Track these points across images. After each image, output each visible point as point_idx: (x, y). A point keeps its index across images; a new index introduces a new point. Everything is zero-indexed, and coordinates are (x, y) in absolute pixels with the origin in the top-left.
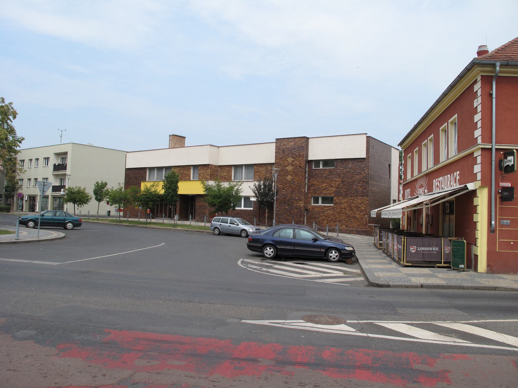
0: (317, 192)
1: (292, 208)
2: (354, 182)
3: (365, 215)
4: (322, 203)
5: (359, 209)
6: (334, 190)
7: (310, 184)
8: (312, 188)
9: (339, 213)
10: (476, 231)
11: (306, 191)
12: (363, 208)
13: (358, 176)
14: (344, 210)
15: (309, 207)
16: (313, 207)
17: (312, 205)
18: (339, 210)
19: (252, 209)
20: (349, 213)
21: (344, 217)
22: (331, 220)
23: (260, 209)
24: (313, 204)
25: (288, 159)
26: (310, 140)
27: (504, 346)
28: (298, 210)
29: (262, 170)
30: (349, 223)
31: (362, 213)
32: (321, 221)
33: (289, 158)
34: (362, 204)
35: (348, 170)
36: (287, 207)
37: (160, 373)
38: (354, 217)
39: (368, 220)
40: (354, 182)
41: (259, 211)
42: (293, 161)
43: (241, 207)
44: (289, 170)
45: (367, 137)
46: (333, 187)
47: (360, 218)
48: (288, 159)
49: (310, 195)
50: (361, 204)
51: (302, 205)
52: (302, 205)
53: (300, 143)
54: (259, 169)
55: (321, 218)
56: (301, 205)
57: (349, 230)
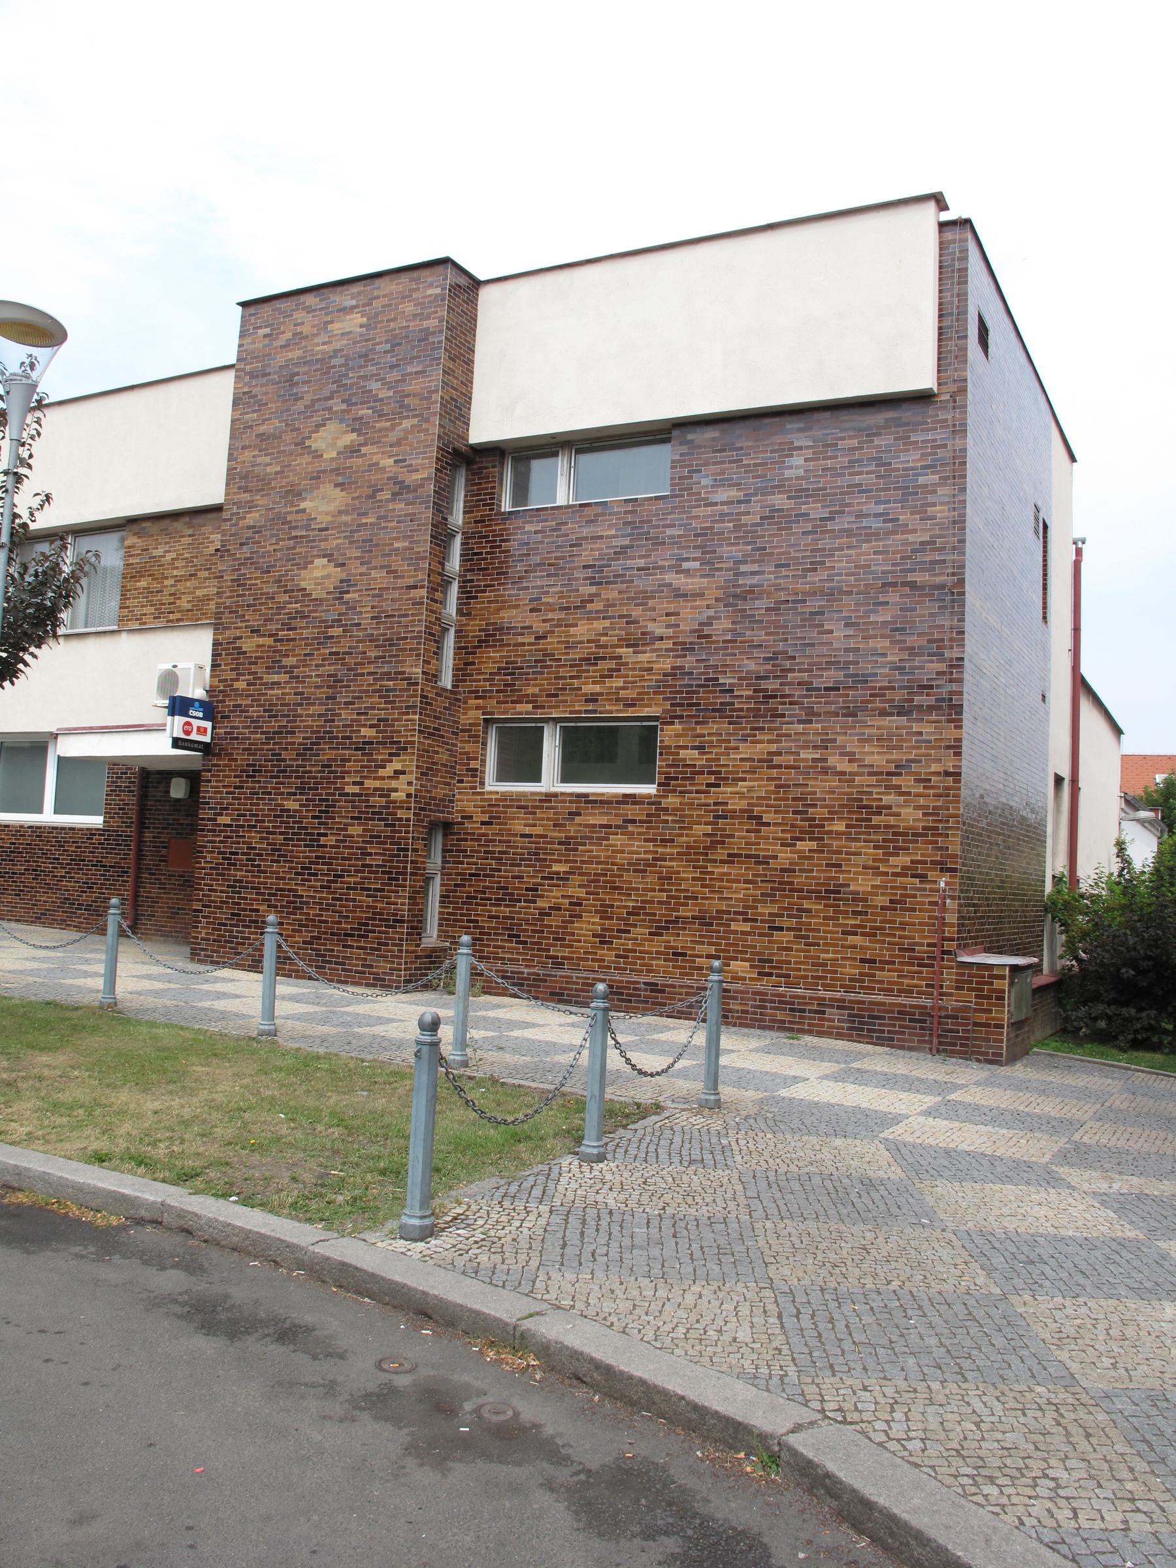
0: (531, 690)
1: (326, 812)
3: (931, 875)
4: (567, 776)
5: (876, 820)
6: (666, 664)
7: (475, 627)
8: (491, 659)
9: (697, 854)
11: (447, 681)
12: (911, 817)
14: (740, 837)
15: (465, 802)
16: (498, 809)
17: (488, 788)
18: (700, 830)
19: (97, 821)
20: (785, 856)
21: (739, 892)
22: (634, 912)
23: (142, 825)
24: (493, 785)
25: (319, 441)
26: (485, 294)
28: (378, 826)
29: (169, 556)
30: (785, 937)
32: (554, 921)
33: (323, 432)
34: (906, 782)
35: (779, 500)
36: (292, 805)
37: (191, 1233)
38: (832, 893)
39: (952, 918)
40: (832, 595)
41: (140, 833)
42: (353, 451)
43: (41, 812)
44: (324, 520)
45: (943, 225)
46: (658, 645)
47: (881, 900)
48: (319, 441)
49: (471, 715)
50: (895, 781)
51: (401, 783)
52: (401, 790)
53: (409, 308)
54: (155, 553)
55: (553, 896)
56: (394, 784)
57: (782, 1002)
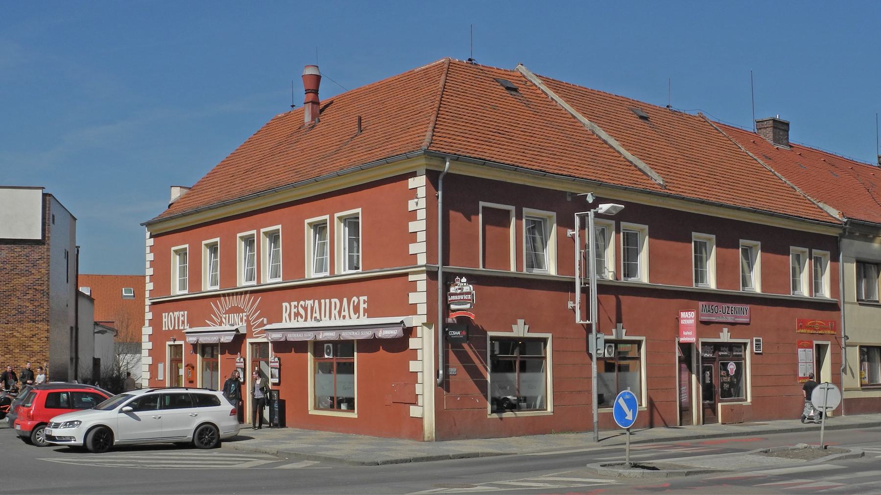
2: (14, 290)
5: (27, 349)
10: (416, 384)
12: (36, 348)
13: (23, 278)
27: (771, 482)
31: (34, 359)
34: (34, 339)
50: (32, 339)
